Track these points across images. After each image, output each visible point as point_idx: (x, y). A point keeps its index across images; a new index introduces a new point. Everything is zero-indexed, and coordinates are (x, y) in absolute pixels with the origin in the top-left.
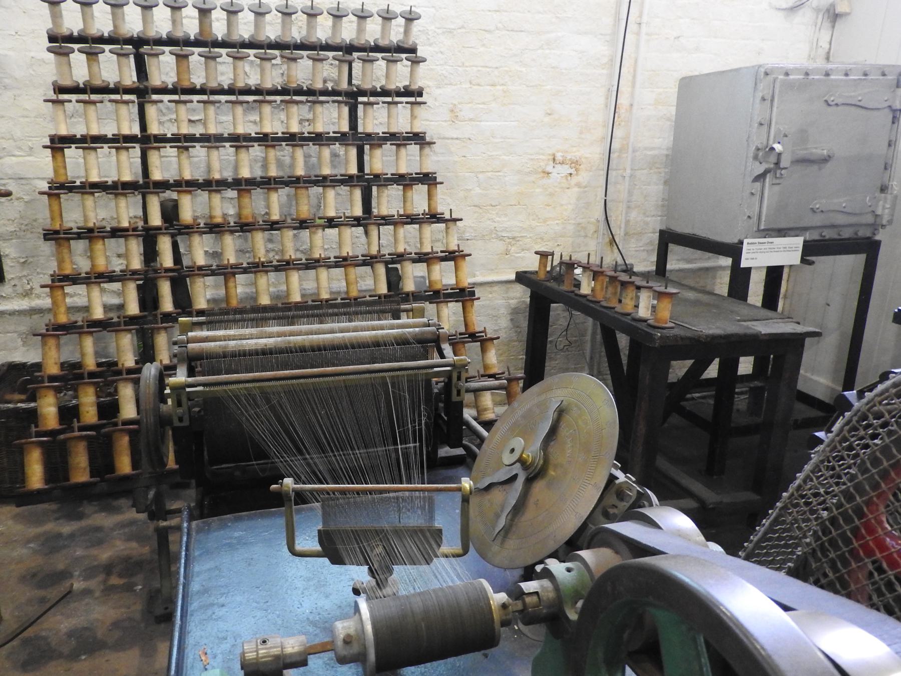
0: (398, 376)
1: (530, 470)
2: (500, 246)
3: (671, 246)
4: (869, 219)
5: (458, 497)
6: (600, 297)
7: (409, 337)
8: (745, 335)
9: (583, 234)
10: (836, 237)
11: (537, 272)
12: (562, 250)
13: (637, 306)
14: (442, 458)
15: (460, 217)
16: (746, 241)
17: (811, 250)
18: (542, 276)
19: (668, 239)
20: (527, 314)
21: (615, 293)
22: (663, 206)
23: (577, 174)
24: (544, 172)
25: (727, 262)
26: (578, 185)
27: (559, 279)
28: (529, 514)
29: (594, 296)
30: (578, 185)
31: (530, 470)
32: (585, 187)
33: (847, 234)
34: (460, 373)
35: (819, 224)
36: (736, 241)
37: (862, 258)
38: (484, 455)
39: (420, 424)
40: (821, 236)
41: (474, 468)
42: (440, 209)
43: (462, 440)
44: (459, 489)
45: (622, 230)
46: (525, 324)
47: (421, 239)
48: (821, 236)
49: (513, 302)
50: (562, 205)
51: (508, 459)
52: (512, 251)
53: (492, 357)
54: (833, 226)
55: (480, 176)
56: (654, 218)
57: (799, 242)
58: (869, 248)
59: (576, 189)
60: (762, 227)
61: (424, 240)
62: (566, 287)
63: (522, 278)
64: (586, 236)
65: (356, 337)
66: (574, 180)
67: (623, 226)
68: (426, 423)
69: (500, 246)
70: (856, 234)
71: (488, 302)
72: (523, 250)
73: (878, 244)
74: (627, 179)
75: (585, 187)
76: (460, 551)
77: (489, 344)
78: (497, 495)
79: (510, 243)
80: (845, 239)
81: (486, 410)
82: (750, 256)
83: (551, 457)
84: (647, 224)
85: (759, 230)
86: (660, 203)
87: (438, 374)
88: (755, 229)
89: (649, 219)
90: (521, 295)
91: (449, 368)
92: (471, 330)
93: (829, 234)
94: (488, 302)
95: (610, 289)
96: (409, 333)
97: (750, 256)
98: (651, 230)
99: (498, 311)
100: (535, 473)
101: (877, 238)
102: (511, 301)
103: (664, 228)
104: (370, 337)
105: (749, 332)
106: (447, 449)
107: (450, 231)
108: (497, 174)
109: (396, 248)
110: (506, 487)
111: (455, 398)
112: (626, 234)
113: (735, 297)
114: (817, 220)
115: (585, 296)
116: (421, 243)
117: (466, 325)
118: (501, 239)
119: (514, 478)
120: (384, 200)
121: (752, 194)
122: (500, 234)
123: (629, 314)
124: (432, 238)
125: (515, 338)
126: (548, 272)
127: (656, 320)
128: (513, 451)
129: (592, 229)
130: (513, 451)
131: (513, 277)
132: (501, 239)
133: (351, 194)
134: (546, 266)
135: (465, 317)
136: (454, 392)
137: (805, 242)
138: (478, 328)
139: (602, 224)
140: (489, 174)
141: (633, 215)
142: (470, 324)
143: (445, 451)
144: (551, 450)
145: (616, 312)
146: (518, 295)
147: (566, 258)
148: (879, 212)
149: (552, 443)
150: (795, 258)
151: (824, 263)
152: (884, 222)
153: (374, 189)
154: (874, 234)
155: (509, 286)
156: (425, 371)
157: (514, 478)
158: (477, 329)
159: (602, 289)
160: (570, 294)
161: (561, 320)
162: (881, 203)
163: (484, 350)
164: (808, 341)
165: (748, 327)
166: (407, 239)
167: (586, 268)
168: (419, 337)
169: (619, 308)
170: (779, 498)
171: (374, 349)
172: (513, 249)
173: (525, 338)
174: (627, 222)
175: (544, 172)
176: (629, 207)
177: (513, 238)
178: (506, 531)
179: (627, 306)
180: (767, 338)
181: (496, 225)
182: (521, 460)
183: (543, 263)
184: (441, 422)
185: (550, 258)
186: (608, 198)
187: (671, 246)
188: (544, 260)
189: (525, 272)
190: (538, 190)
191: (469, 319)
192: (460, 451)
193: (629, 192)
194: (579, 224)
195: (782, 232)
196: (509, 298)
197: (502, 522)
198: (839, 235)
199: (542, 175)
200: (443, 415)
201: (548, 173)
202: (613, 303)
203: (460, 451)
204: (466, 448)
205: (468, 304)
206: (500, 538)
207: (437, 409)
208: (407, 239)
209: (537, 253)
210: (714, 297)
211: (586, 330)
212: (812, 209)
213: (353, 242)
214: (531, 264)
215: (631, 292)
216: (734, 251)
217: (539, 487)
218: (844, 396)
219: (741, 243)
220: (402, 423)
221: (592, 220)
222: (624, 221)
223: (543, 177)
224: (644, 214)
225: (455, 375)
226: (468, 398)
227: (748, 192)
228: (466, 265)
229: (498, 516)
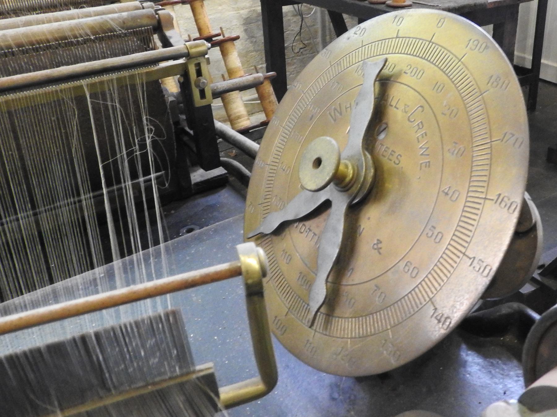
1: (354, 190)
5: (237, 288)
14: (197, 184)
20: (260, 23)
31: (354, 190)
34: (198, 65)
38: (260, 176)
39: (143, 146)
41: (248, 197)
44: (236, 272)
46: (260, 34)
49: (244, 13)
51: (313, 179)
53: (235, 59)
65: (26, 35)
71: (219, 15)
76: (261, 387)
77: (228, 45)
78: (299, 240)
81: (239, 117)
87: (168, 72)
91: (181, 61)
92: (206, 34)
94: (219, 15)
96: (112, 19)
100: (363, 191)
102: (242, 12)
104: (51, 32)
106: (201, 171)
110: (311, 223)
111: (198, 102)
117: (200, 30)
119: (327, 205)
125: (252, 48)
128: (318, 162)
130: (318, 162)
135: (196, 21)
136: (196, 93)
138: (214, 31)
143: (198, 175)
144: (380, 149)
149: (382, 136)
156: (144, 70)
158: (214, 32)
161: (293, 25)
163: (224, 54)
168: (130, 24)
170: (177, 150)
173: (262, 47)
178: (332, 301)
182: (338, 180)
184: (186, 138)
191: (201, 22)
192: (219, 171)
196: (238, 9)
197: (320, 292)
200: (187, 129)
203: (219, 171)
204: (226, 165)
206: (321, 319)
207: (177, 123)
211: (316, 32)
217: (372, 218)
225: (192, 70)
226: (217, 104)
229: (308, 282)
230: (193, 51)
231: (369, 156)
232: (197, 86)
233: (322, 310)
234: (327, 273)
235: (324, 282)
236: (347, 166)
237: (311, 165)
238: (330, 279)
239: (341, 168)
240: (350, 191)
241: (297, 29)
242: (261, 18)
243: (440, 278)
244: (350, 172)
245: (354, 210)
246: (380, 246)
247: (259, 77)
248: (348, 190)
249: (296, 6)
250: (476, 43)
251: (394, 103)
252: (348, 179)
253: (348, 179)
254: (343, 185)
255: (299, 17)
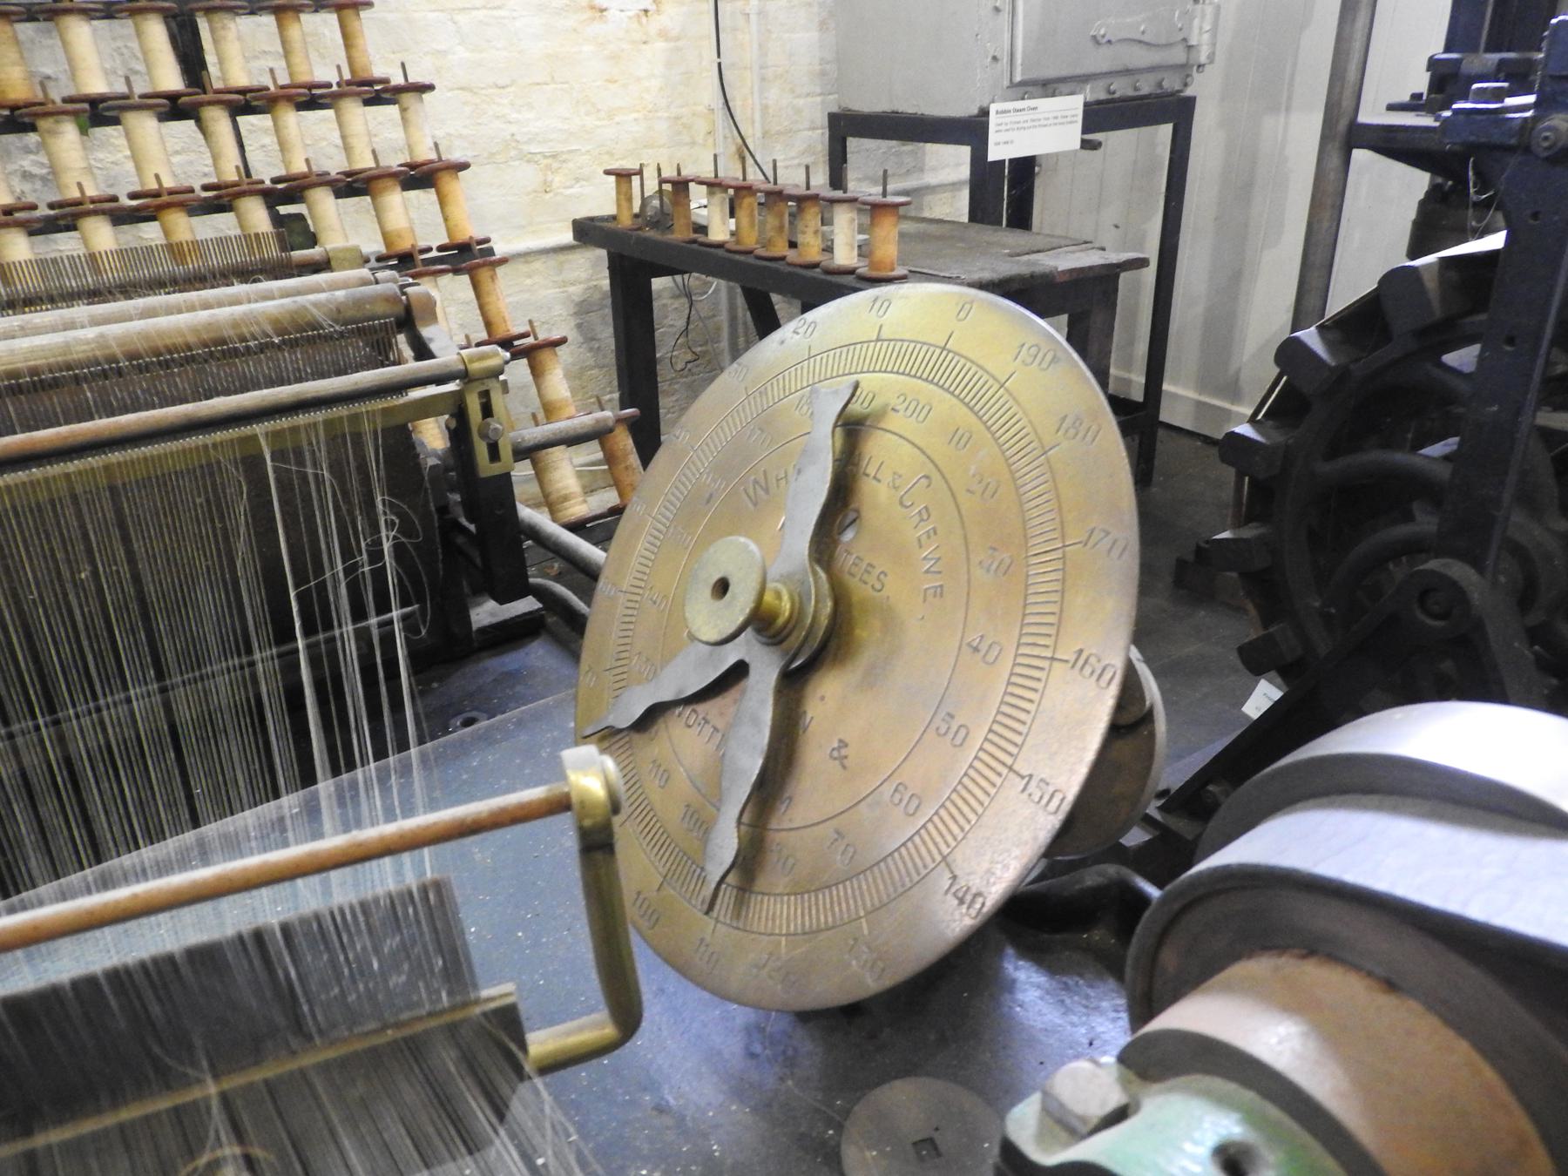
0: (295, 430)
2: (528, 176)
3: (853, 143)
4: (1178, 56)
5: (563, 836)
6: (750, 240)
7: (319, 315)
8: (1032, 276)
9: (687, 139)
10: (1131, 93)
11: (614, 218)
12: (659, 159)
13: (829, 249)
15: (426, 80)
16: (993, 108)
17: (1099, 118)
18: (626, 221)
19: (845, 127)
21: (781, 228)
22: (823, 73)
23: (658, 12)
24: (592, 8)
25: (965, 152)
26: (663, 34)
27: (661, 221)
28: (814, 795)
29: (738, 242)
30: (663, 34)
32: (678, 39)
33: (1146, 87)
34: (486, 395)
35: (1105, 68)
36: (975, 111)
37: (1166, 130)
38: (607, 615)
39: (376, 555)
40: (1110, 92)
41: (586, 656)
42: (378, 71)
43: (527, 577)
45: (758, 125)
47: (344, 137)
48: (1110, 92)
49: (576, 291)
50: (639, 80)
51: (711, 620)
52: (555, 185)
53: (558, 384)
54: (1127, 72)
55: (461, 18)
56: (810, 99)
57: (1072, 106)
58: (1176, 111)
59: (660, 45)
60: (1018, 78)
61: (354, 141)
62: (680, 234)
63: (587, 232)
64: (693, 143)
66: (656, 23)
67: (757, 117)
68: (398, 549)
69: (528, 176)
70: (1160, 85)
71: (526, 296)
72: (577, 180)
73: (1190, 103)
74: (753, 18)
75: (678, 39)
76: (609, 1031)
77: (545, 356)
78: (685, 740)
79: (548, 167)
80: (1142, 98)
81: (566, 498)
82: (1003, 137)
83: (853, 583)
84: (798, 111)
85: (1013, 85)
86: (818, 68)
87: (426, 408)
88: (1006, 83)
89: (801, 102)
90: (591, 272)
91: (451, 387)
93: (1122, 88)
94: (526, 296)
95: (772, 221)
97: (1003, 137)
98: (807, 124)
99: (553, 293)
101: (1189, 92)
102: (572, 289)
103: (835, 109)
104: (195, 330)
105: (1038, 269)
107: (410, 114)
108: (495, 13)
109: (286, 163)
112: (765, 134)
113: (981, 221)
114: (1100, 61)
115: (720, 246)
116: (347, 148)
118: (530, 158)
119: (739, 671)
120: (233, 49)
121: (997, 10)
122: (526, 148)
123: (816, 265)
124: (378, 136)
126: (636, 216)
127: (872, 265)
128: (722, 587)
129: (702, 126)
130: (722, 587)
131: (568, 237)
132: (530, 158)
133: (139, 34)
134: (630, 199)
135: (481, 307)
136: (481, 449)
137: (1086, 105)
139: (720, 114)
140: (480, 14)
141: (774, 94)
142: (495, 319)
143: (486, 613)
145: (789, 264)
146: (584, 276)
147: (669, 172)
148: (1193, 42)
149: (848, 535)
150: (1069, 136)
151: (1118, 141)
152: (1203, 59)
153: (203, 25)
154: (1186, 85)
155: (561, 257)
156: (379, 404)
157: (739, 671)
158: (517, 330)
159: (752, 224)
160: (695, 246)
162: (1196, 22)
163: (537, 372)
164: (1124, 278)
165: (1035, 263)
166: (314, 141)
167: (714, 185)
168: (350, 313)
169: (791, 255)
171: (215, 360)
172: (558, 180)
173: (611, 359)
174: (765, 108)
175: (592, 8)
176: (763, 79)
177: (554, 156)
179: (811, 250)
180: (1066, 278)
181: (513, 129)
182: (761, 622)
183: (624, 195)
184: (460, 540)
185: (636, 180)
186: (722, 60)
187: (853, 143)
188: (624, 187)
189: (592, 219)
190: (587, 48)
191: (492, 310)
192: (527, 605)
193: (760, 46)
194: (677, 118)
195: (1048, 87)
196: (565, 284)
197: (726, 844)
198: (1136, 89)
199: (589, 14)
201: (603, 10)
202: (780, 249)
203: (527, 605)
204: (540, 593)
205: (484, 274)
206: (727, 897)
207: (443, 510)
208: (314, 141)
209: (608, 173)
210: (948, 227)
211: (718, 329)
212: (1094, 37)
213: (173, 154)
214: (600, 201)
215: (812, 218)
216: (972, 131)
217: (828, 697)
218: (1297, 339)
219: (985, 113)
220: (309, 563)
221: (700, 108)
222: (758, 107)
223: (593, 19)
224: (792, 91)
226: (522, 471)
227: (990, 5)
228: (461, 187)
229: (703, 826)
230: (475, 367)
231: (822, 575)
232: (484, 436)
233: (731, 879)
234: (740, 806)
235: (733, 824)
236: (778, 596)
237: (708, 592)
238: (745, 819)
239: (769, 598)
240: (785, 645)
241: (681, 323)
242: (609, 301)
243: (964, 816)
244: (786, 606)
245: (793, 681)
246: (844, 752)
247: (605, 419)
248: (781, 642)
249: (678, 278)
250: (1034, 350)
251: (871, 470)
252: (781, 621)
253: (781, 621)
254: (772, 631)
255: (684, 300)
